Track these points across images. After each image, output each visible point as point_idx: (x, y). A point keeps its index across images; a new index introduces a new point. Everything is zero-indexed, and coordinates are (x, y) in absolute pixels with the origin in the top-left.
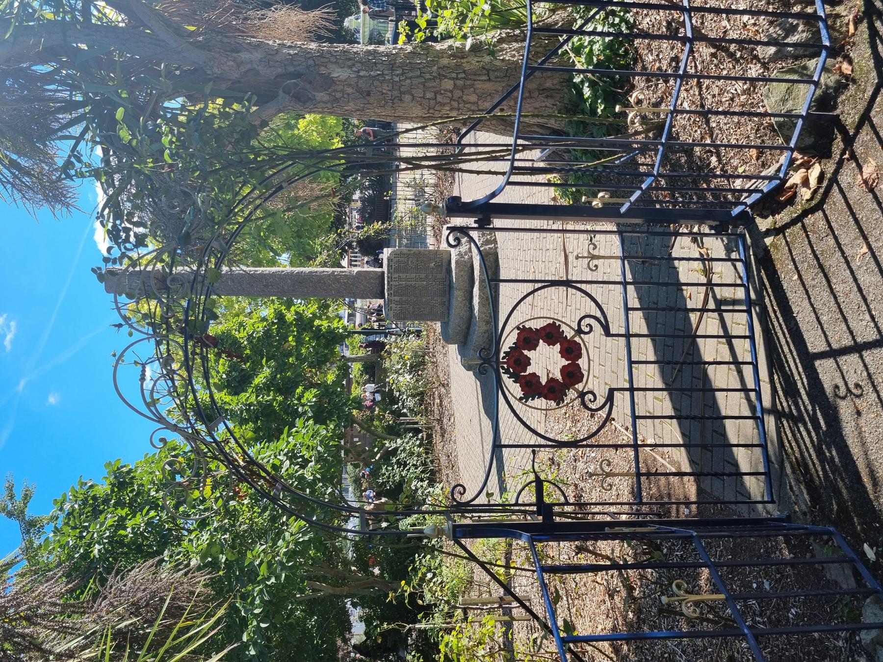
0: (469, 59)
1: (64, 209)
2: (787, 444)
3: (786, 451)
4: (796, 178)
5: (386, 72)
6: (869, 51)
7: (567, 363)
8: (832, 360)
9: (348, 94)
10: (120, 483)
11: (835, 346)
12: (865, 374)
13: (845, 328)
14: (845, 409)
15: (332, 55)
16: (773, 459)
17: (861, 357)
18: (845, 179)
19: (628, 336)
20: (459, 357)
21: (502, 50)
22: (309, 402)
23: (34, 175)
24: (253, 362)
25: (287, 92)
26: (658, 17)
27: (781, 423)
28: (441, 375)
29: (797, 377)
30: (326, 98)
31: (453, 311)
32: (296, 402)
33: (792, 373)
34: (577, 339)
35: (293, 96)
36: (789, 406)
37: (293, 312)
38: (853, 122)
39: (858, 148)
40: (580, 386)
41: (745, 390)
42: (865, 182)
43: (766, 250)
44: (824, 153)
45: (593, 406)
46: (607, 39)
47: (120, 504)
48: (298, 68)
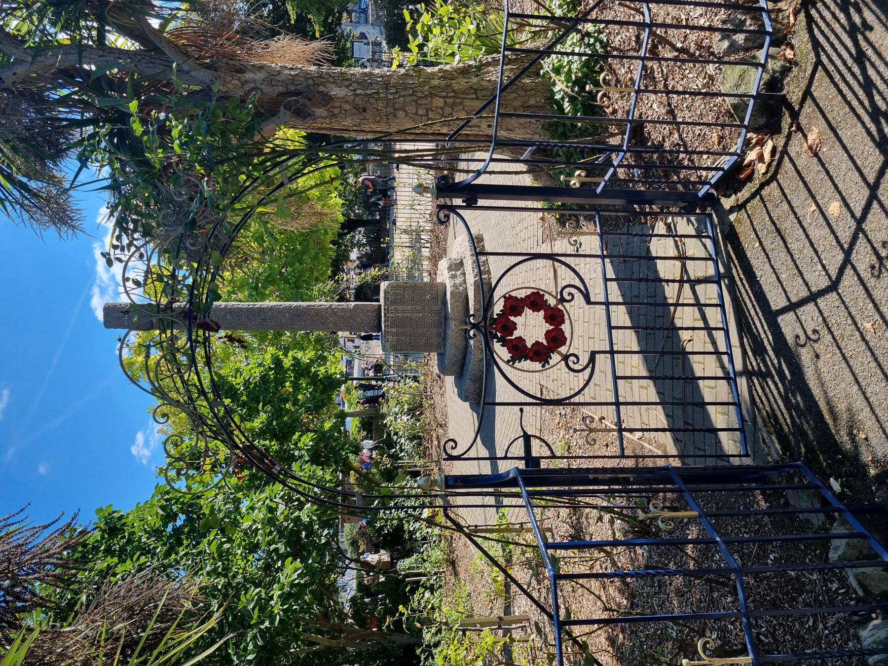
0: (459, 80)
1: (70, 232)
2: (758, 400)
3: (757, 407)
4: (752, 156)
5: (381, 91)
6: (807, 36)
7: (551, 327)
8: (792, 313)
9: (346, 111)
10: (110, 528)
11: (794, 300)
12: (821, 319)
13: (801, 281)
14: (805, 356)
15: (331, 76)
16: (747, 418)
17: (816, 305)
18: (793, 150)
19: (607, 304)
20: (456, 390)
21: (488, 72)
22: (306, 445)
23: (42, 197)
24: (249, 409)
25: (288, 107)
26: (628, 34)
27: (752, 381)
28: (438, 416)
29: (763, 336)
30: (325, 114)
31: (449, 341)
32: (292, 446)
33: (759, 333)
34: (560, 307)
35: (293, 112)
36: (758, 364)
37: (290, 358)
38: (797, 99)
39: (803, 120)
40: (563, 350)
41: (717, 353)
42: (810, 148)
43: (732, 226)
44: (773, 129)
45: (576, 367)
46: (584, 58)
47: (109, 552)
48: (298, 87)
